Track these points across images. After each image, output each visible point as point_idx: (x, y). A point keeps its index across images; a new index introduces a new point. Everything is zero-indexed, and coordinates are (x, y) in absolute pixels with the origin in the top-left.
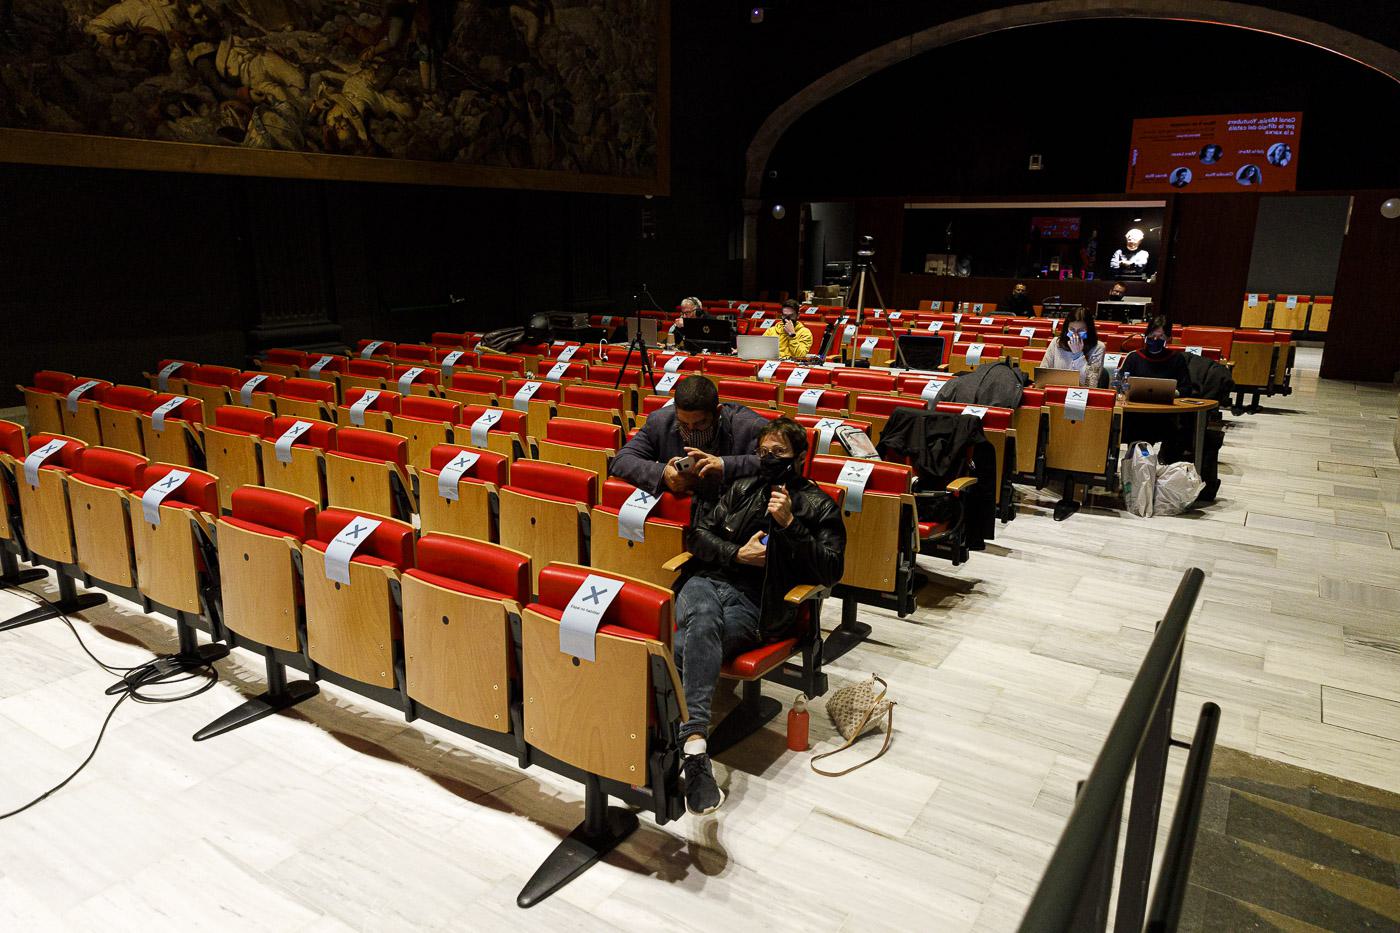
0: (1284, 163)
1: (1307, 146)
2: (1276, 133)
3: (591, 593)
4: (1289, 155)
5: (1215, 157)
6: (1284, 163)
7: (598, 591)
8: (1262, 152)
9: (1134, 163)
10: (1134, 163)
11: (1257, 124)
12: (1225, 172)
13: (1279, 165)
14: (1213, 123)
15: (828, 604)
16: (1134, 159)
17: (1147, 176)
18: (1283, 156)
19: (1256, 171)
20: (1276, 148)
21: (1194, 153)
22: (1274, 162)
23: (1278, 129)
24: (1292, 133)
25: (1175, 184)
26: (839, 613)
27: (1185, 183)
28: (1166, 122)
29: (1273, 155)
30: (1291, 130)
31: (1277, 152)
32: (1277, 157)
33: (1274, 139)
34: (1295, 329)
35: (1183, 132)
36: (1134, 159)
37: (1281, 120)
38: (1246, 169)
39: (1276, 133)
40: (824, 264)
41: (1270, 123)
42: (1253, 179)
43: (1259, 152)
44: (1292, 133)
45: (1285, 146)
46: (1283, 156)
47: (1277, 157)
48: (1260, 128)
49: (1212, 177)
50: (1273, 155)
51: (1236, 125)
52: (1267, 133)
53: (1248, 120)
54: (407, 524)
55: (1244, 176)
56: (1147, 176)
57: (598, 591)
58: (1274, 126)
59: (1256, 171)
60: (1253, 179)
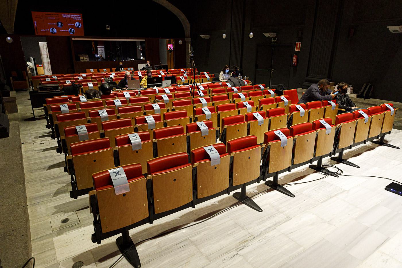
0: (80, 27)
1: (85, 21)
2: (76, 19)
3: (211, 151)
4: (81, 25)
5: (61, 25)
6: (80, 27)
7: (210, 150)
8: (74, 24)
9: (36, 26)
10: (36, 26)
11: (70, 16)
12: (65, 30)
13: (79, 27)
14: (58, 15)
15: (140, 249)
16: (36, 24)
17: (41, 30)
18: (79, 25)
19: (73, 30)
20: (77, 23)
21: (55, 24)
22: (77, 27)
23: (76, 18)
24: (80, 19)
25: (52, 33)
26: (141, 260)
27: (55, 33)
28: (44, 13)
29: (77, 25)
30: (80, 18)
31: (77, 24)
32: (78, 25)
33: (77, 21)
34: (31, 106)
35: (51, 17)
36: (36, 24)
37: (77, 16)
38: (71, 30)
39: (76, 19)
40: (101, 43)
41: (74, 16)
42: (73, 32)
43: (73, 24)
44: (80, 19)
45: (79, 23)
46: (79, 25)
47: (78, 25)
48: (72, 17)
49: (62, 31)
50: (77, 25)
51: (65, 16)
52: (74, 19)
53: (68, 15)
54: (154, 116)
55: (70, 31)
56: (41, 30)
57: (210, 150)
58: (75, 17)
59: (73, 30)
60: (73, 32)
